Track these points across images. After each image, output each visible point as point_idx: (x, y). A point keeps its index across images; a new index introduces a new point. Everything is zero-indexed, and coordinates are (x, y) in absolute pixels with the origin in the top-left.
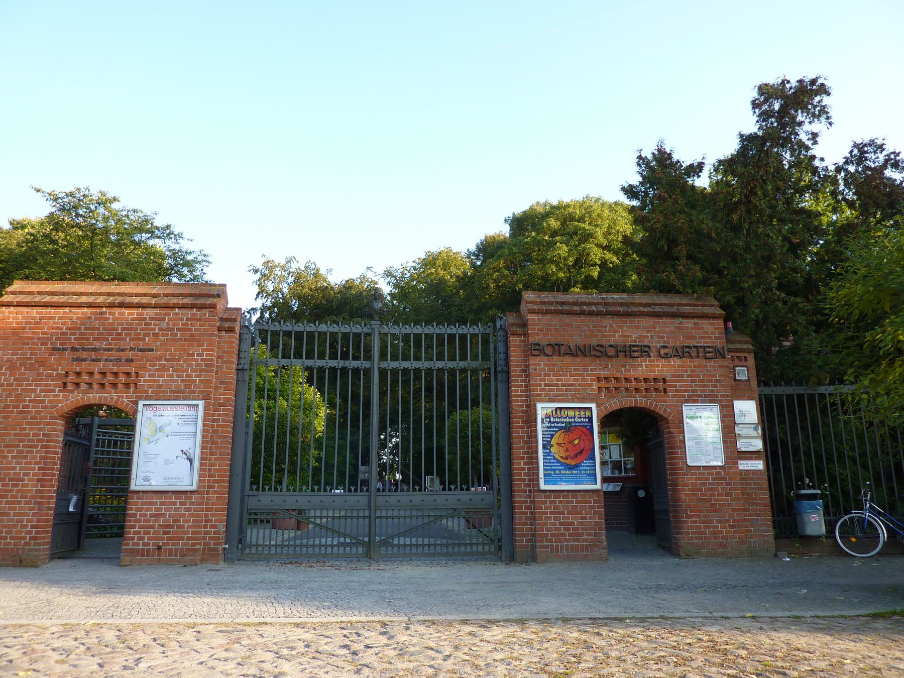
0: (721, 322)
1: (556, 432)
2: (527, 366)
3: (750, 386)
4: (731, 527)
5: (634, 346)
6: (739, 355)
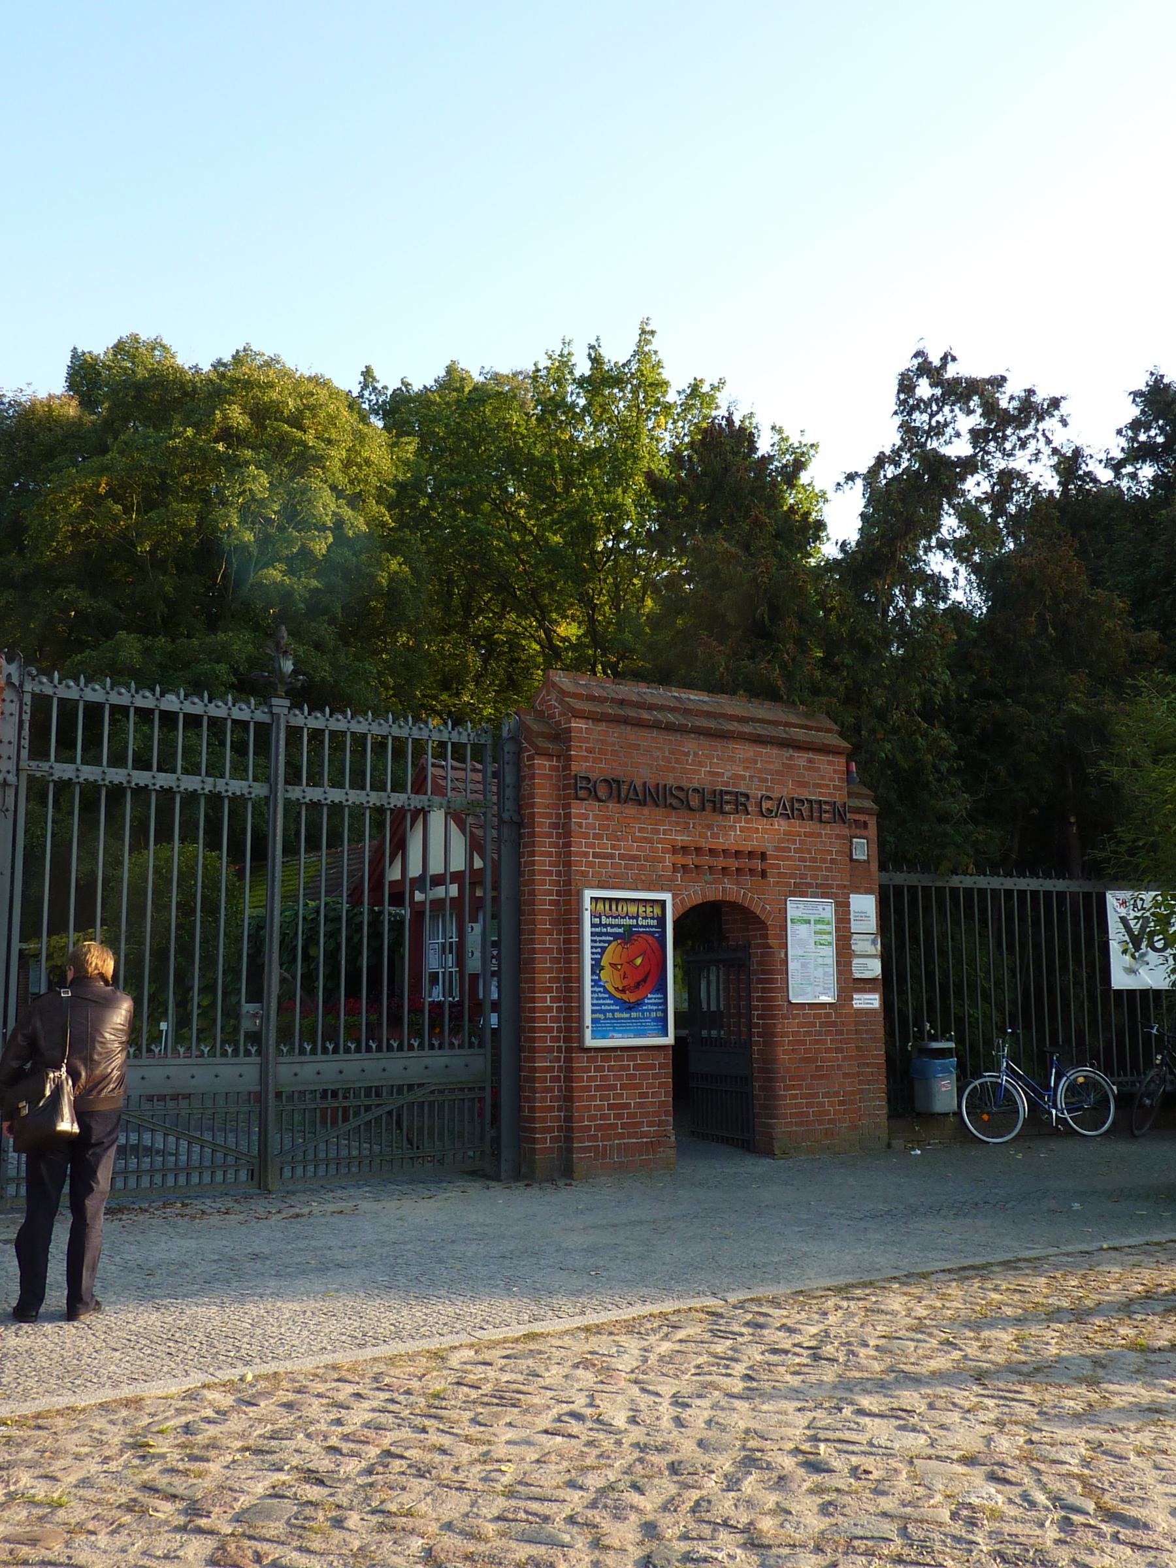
0: (843, 760)
1: (609, 942)
2: (568, 816)
3: (869, 870)
4: (841, 1103)
5: (727, 793)
6: (857, 817)
